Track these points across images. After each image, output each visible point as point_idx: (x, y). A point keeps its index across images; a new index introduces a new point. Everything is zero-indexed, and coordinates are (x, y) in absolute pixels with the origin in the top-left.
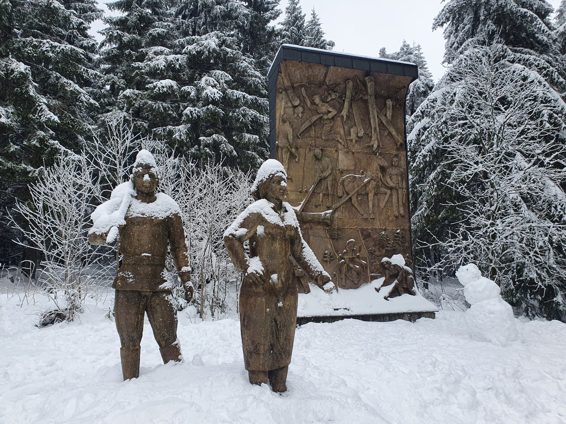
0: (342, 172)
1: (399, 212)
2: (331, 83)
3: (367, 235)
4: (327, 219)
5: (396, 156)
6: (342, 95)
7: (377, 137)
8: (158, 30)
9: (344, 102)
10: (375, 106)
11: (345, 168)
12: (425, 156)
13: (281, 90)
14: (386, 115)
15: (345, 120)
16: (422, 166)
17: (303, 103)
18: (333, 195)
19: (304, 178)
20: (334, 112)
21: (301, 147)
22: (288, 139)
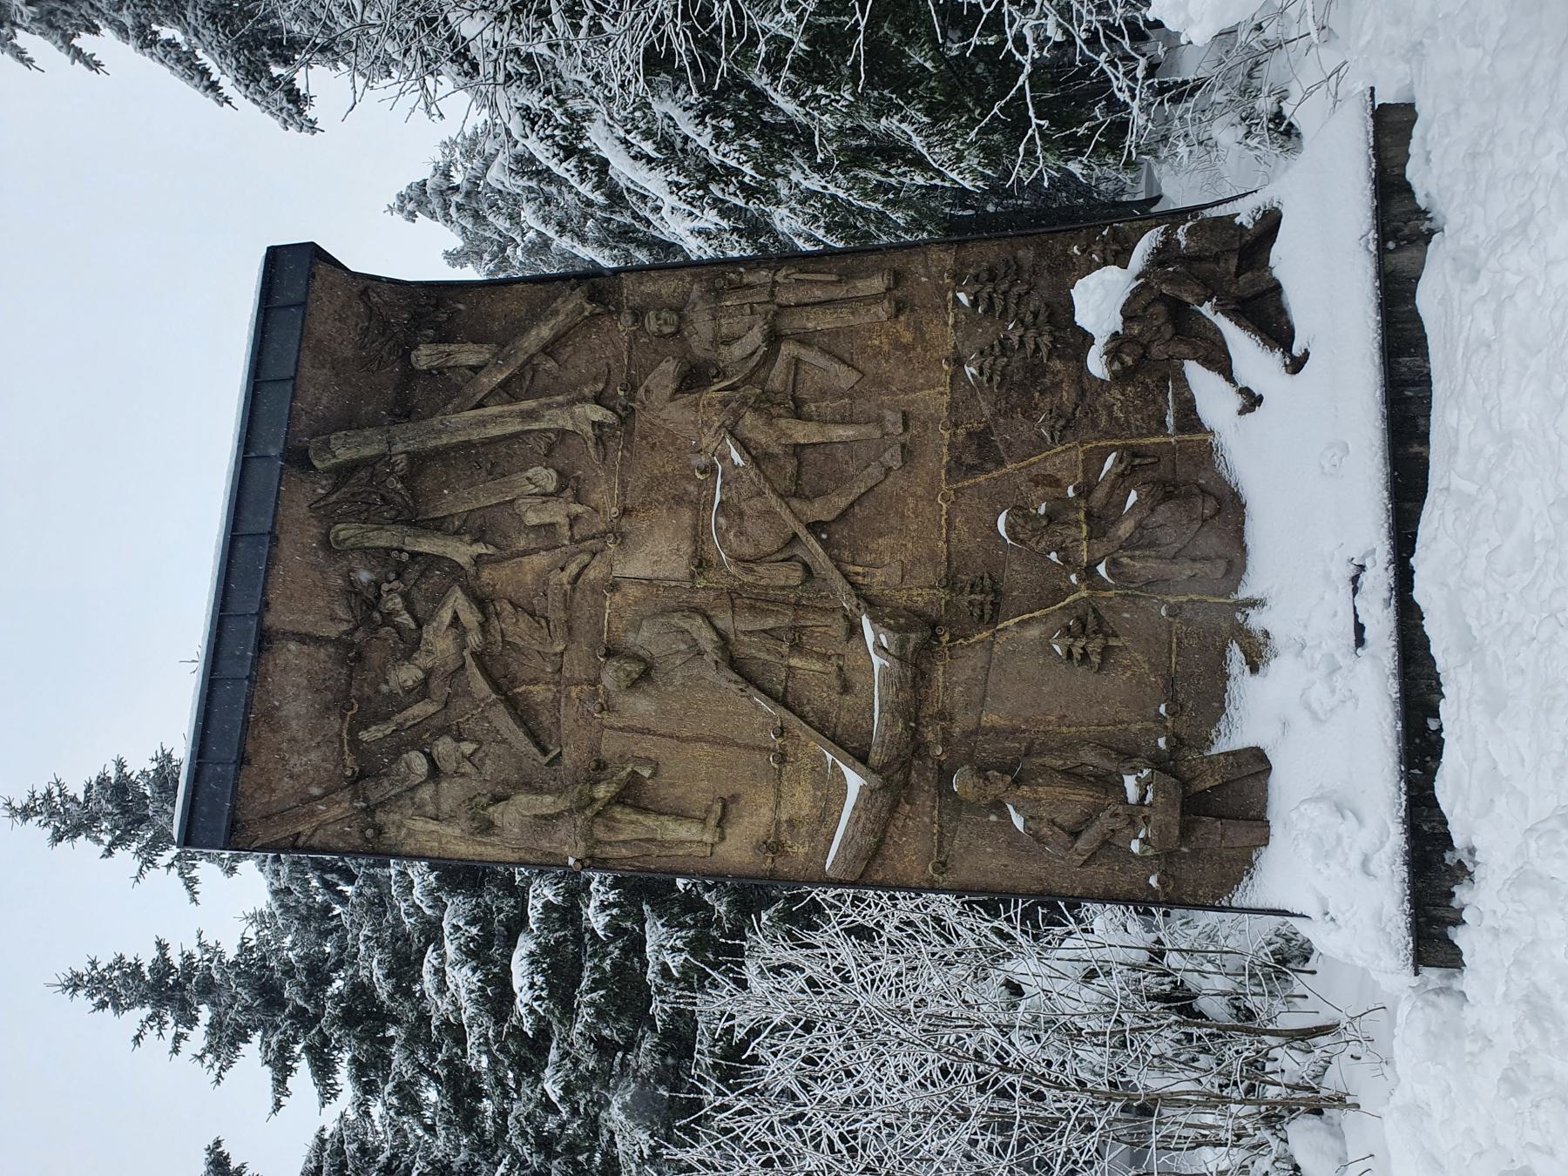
0: (701, 563)
1: (876, 299)
2: (341, 612)
3: (981, 450)
4: (902, 647)
5: (638, 314)
6: (396, 564)
7: (560, 405)
8: (374, 970)
9: (421, 554)
10: (435, 421)
11: (686, 547)
12: (719, 135)
13: (369, 833)
14: (476, 369)
15: (491, 550)
16: (753, 143)
17: (418, 736)
18: (797, 605)
19: (725, 742)
20: (457, 601)
21: (595, 750)
22: (558, 816)
